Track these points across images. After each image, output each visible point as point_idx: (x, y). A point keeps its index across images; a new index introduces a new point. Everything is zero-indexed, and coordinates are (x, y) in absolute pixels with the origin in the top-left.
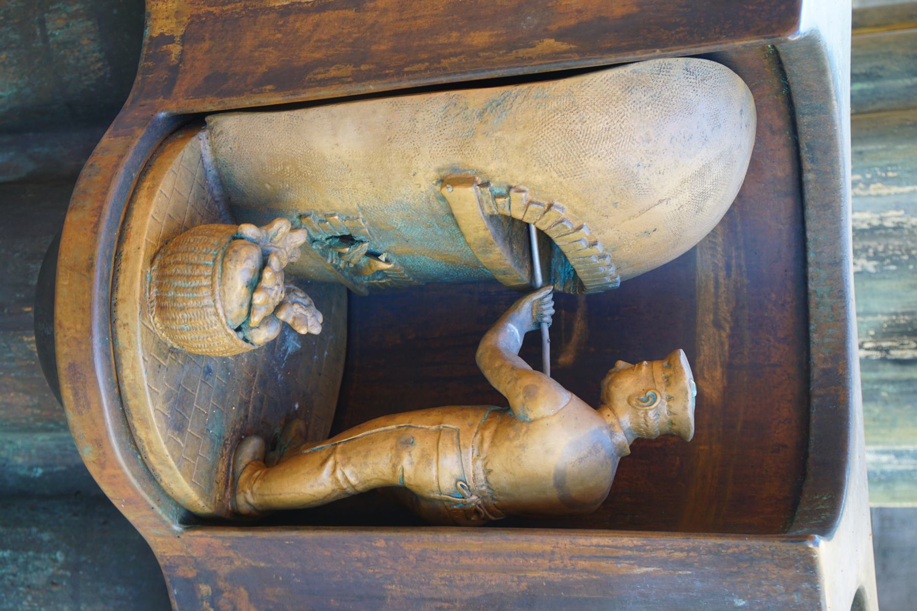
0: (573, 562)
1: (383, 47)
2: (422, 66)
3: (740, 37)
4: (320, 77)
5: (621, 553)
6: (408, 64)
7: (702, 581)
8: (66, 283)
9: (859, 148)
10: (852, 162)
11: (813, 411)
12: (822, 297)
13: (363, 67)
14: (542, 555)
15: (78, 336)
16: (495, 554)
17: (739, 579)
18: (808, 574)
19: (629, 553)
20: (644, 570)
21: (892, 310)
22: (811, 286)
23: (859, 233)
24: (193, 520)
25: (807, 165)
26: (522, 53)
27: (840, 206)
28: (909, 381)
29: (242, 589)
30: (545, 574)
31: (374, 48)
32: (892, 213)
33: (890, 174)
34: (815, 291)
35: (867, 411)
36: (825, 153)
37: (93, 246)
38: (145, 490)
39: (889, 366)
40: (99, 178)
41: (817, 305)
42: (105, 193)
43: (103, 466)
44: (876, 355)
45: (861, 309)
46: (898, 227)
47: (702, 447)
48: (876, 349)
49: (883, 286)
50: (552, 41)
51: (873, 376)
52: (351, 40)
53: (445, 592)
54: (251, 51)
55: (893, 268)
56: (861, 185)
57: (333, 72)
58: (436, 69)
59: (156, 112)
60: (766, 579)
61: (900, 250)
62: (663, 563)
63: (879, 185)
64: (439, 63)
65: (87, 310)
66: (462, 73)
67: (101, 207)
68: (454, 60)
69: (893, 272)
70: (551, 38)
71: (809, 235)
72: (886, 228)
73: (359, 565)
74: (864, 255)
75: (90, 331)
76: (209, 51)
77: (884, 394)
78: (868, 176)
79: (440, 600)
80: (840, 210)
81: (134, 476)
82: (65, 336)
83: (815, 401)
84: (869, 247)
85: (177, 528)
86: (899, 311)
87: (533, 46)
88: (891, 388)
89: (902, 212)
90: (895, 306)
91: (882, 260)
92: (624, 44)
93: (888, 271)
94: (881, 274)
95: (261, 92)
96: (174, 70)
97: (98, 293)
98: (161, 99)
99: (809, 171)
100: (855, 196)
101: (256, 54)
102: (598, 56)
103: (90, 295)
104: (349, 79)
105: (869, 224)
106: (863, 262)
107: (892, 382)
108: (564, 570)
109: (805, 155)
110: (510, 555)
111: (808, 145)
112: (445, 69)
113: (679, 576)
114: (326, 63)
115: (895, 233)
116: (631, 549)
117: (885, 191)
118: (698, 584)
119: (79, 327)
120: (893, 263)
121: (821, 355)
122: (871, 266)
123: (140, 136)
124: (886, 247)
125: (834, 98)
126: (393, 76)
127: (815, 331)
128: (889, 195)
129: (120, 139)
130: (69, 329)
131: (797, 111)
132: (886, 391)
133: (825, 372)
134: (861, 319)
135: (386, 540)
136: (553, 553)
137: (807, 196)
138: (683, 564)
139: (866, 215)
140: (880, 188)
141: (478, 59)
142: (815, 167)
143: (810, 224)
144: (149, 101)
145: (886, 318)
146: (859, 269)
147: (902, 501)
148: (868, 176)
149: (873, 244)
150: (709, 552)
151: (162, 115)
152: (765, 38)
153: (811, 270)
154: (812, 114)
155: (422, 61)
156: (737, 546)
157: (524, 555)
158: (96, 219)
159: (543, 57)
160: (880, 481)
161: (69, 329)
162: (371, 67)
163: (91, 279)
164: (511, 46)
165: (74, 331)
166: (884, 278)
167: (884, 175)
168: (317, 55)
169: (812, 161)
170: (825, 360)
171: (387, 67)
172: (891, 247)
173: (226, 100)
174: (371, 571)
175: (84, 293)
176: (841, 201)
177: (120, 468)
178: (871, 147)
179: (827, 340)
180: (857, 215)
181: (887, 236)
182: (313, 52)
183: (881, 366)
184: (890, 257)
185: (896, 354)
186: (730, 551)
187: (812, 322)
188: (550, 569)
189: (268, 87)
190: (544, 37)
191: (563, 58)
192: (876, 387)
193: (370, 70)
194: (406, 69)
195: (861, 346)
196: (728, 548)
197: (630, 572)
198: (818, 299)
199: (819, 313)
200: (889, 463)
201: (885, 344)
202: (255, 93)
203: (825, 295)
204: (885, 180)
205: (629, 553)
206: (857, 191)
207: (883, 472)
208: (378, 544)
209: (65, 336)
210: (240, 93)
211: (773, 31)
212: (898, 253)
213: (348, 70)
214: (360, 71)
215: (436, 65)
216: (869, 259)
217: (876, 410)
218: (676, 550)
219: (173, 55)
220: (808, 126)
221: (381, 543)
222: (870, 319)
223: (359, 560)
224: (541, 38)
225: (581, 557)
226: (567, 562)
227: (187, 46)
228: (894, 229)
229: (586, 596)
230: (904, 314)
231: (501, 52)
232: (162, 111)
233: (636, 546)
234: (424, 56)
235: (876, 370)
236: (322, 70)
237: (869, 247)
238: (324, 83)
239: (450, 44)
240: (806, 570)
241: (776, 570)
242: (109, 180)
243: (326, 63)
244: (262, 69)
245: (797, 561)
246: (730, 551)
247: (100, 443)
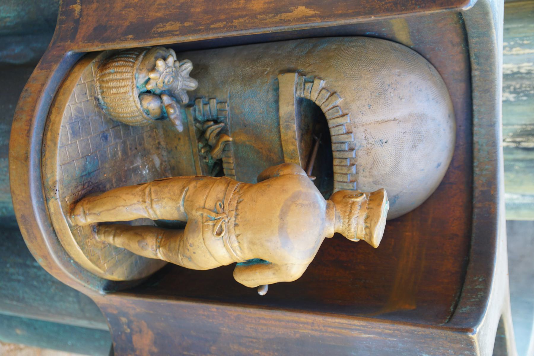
0: (325, 328)
1: (198, 10)
2: (221, 25)
3: (429, 8)
4: (160, 30)
5: (354, 327)
6: (212, 23)
7: (403, 344)
8: (14, 167)
9: (508, 26)
10: (503, 81)
11: (475, 217)
12: (482, 145)
13: (186, 24)
14: (307, 323)
15: (24, 199)
16: (279, 320)
17: (426, 345)
18: (469, 347)
19: (358, 328)
20: (367, 336)
21: (523, 122)
22: (475, 139)
23: (506, 77)
24: (113, 287)
25: (474, 66)
26: (284, 16)
27: (495, 91)
28: (531, 161)
29: (143, 322)
30: (310, 332)
31: (193, 10)
32: (526, 64)
33: (525, 42)
34: (478, 142)
35: (506, 176)
36: (487, 60)
37: (28, 144)
38: (78, 278)
39: (520, 152)
40: (30, 99)
41: (479, 150)
42: (33, 110)
43: (51, 268)
44: (513, 145)
45: (505, 122)
46: (529, 73)
47: (407, 234)
48: (513, 142)
49: (518, 109)
50: (304, 8)
51: (511, 157)
52: (179, 5)
53: (254, 335)
54: (120, 10)
55: (525, 98)
56: (508, 49)
57: (168, 27)
58: (231, 27)
59: (66, 52)
60: (442, 347)
61: (529, 87)
62: (379, 334)
63: (518, 48)
64: (232, 22)
65: (27, 184)
66: (246, 30)
67: (31, 120)
68: (241, 20)
69: (525, 101)
70: (303, 6)
71: (475, 108)
72: (521, 73)
73: (204, 317)
74: (508, 90)
75: (30, 197)
76: (96, 10)
77: (517, 168)
78: (512, 43)
79: (251, 338)
80: (495, 94)
81: (71, 273)
82: (17, 199)
83: (476, 211)
84: (511, 86)
85: (102, 292)
86: (528, 123)
87: (291, 11)
88: (521, 164)
89: (531, 64)
90: (525, 120)
91: (518, 93)
92: (350, 11)
93: (522, 100)
94: (518, 102)
95: (126, 40)
96: (77, 22)
97: (33, 174)
98: (69, 43)
99: (476, 70)
100: (504, 55)
101: (123, 13)
102: (333, 19)
103: (28, 176)
104: (178, 33)
105: (511, 71)
106: (507, 95)
107: (522, 161)
108: (320, 331)
109: (473, 60)
110: (288, 321)
111: (475, 55)
112: (235, 27)
113: (389, 340)
114: (163, 20)
115: (527, 76)
116: (360, 326)
117: (522, 52)
118: (400, 345)
119: (24, 194)
120: (525, 95)
121: (480, 182)
122: (511, 97)
123: (55, 70)
124: (521, 85)
125: (494, 27)
126: (203, 31)
127: (477, 167)
128: (524, 54)
129: (43, 71)
130: (18, 195)
131: (469, 35)
132: (518, 166)
133: (483, 192)
134: (505, 127)
135: (217, 309)
136: (313, 323)
137: (474, 85)
138: (391, 335)
139: (510, 66)
140: (519, 50)
141: (256, 20)
142: (479, 67)
143: (476, 101)
144: (62, 44)
145: (519, 127)
146: (505, 99)
147: (525, 216)
148: (512, 43)
149: (513, 83)
150: (407, 332)
151: (69, 53)
152: (446, 9)
153: (475, 129)
154: (478, 37)
155: (221, 21)
156: (424, 332)
157: (296, 322)
158: (28, 128)
159: (298, 20)
160: (512, 209)
161: (18, 195)
162: (191, 24)
163: (27, 166)
164: (277, 11)
165: (21, 196)
166: (519, 105)
167: (521, 42)
168: (159, 15)
169: (478, 64)
170: (483, 185)
171: (200, 24)
172: (524, 86)
173: (106, 44)
174: (211, 321)
175: (24, 175)
176: (496, 88)
177: (60, 269)
178: (514, 26)
179: (484, 173)
180: (506, 66)
181: (522, 78)
182: (156, 12)
183: (515, 151)
184: (523, 92)
185: (524, 145)
186: (420, 333)
187: (475, 161)
188: (312, 330)
189: (131, 36)
190: (298, 5)
191: (310, 21)
192: (512, 163)
193: (190, 26)
194: (212, 26)
195: (504, 141)
196: (419, 332)
197: (360, 336)
198: (479, 147)
199: (480, 155)
200: (517, 199)
201: (518, 139)
202: (122, 40)
203: (484, 145)
204: (522, 46)
205: (358, 328)
206: (506, 52)
207: (514, 204)
208: (213, 310)
209: (17, 199)
210: (113, 40)
211: (452, 4)
212: (528, 89)
213: (177, 25)
214: (184, 26)
215: (230, 24)
216: (511, 93)
217: (512, 176)
218: (386, 329)
219: (76, 12)
220: (476, 43)
221: (215, 310)
222: (510, 127)
223: (204, 315)
224: (296, 5)
225: (330, 327)
226: (321, 328)
227: (84, 6)
228: (527, 73)
229: (334, 344)
230: (530, 125)
231: (271, 16)
232: (70, 51)
233: (362, 325)
234: (223, 17)
235: (512, 154)
236: (162, 25)
237: (511, 86)
238: (162, 35)
239: (239, 8)
240: (467, 345)
241: (449, 344)
242: (36, 102)
243: (163, 20)
244: (127, 23)
245: (462, 341)
246: (420, 333)
247: (46, 257)
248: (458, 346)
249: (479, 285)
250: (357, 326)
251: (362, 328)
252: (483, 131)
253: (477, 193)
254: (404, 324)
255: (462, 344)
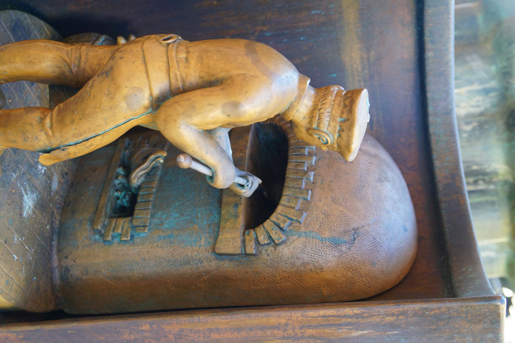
12: (439, 136)
14: (277, 327)
22: (432, 129)
34: (434, 133)
62: (376, 326)
83: (443, 205)
110: (251, 329)
113: (388, 336)
135: (151, 324)
136: (286, 324)
157: (263, 328)
186: (433, 312)
196: (432, 310)
248: (480, 327)
249: (471, 274)
250: (351, 317)
251: (354, 320)
252: (439, 120)
253: (440, 187)
254: (412, 302)
255: (485, 323)
